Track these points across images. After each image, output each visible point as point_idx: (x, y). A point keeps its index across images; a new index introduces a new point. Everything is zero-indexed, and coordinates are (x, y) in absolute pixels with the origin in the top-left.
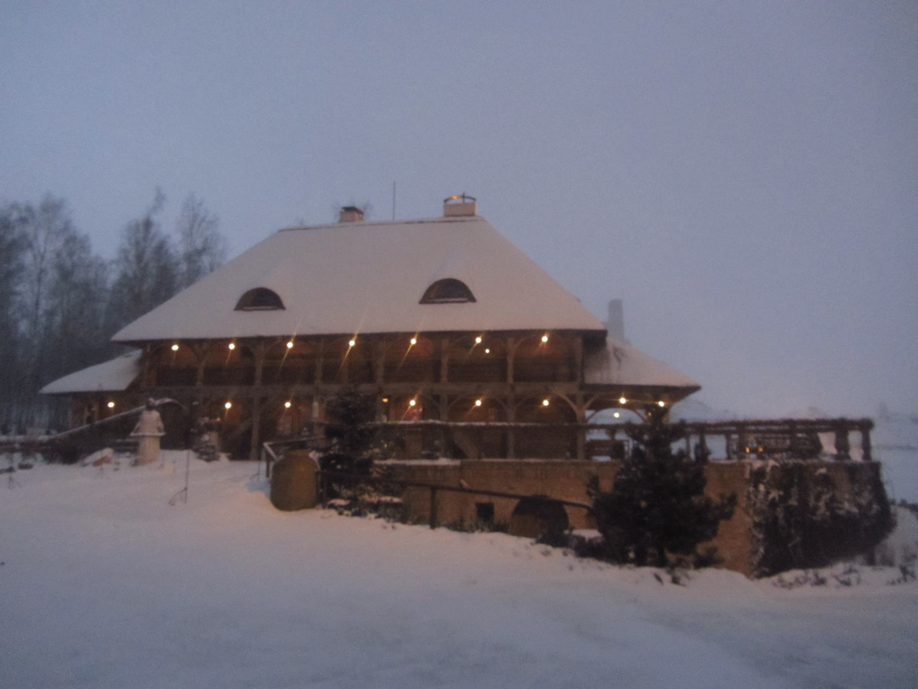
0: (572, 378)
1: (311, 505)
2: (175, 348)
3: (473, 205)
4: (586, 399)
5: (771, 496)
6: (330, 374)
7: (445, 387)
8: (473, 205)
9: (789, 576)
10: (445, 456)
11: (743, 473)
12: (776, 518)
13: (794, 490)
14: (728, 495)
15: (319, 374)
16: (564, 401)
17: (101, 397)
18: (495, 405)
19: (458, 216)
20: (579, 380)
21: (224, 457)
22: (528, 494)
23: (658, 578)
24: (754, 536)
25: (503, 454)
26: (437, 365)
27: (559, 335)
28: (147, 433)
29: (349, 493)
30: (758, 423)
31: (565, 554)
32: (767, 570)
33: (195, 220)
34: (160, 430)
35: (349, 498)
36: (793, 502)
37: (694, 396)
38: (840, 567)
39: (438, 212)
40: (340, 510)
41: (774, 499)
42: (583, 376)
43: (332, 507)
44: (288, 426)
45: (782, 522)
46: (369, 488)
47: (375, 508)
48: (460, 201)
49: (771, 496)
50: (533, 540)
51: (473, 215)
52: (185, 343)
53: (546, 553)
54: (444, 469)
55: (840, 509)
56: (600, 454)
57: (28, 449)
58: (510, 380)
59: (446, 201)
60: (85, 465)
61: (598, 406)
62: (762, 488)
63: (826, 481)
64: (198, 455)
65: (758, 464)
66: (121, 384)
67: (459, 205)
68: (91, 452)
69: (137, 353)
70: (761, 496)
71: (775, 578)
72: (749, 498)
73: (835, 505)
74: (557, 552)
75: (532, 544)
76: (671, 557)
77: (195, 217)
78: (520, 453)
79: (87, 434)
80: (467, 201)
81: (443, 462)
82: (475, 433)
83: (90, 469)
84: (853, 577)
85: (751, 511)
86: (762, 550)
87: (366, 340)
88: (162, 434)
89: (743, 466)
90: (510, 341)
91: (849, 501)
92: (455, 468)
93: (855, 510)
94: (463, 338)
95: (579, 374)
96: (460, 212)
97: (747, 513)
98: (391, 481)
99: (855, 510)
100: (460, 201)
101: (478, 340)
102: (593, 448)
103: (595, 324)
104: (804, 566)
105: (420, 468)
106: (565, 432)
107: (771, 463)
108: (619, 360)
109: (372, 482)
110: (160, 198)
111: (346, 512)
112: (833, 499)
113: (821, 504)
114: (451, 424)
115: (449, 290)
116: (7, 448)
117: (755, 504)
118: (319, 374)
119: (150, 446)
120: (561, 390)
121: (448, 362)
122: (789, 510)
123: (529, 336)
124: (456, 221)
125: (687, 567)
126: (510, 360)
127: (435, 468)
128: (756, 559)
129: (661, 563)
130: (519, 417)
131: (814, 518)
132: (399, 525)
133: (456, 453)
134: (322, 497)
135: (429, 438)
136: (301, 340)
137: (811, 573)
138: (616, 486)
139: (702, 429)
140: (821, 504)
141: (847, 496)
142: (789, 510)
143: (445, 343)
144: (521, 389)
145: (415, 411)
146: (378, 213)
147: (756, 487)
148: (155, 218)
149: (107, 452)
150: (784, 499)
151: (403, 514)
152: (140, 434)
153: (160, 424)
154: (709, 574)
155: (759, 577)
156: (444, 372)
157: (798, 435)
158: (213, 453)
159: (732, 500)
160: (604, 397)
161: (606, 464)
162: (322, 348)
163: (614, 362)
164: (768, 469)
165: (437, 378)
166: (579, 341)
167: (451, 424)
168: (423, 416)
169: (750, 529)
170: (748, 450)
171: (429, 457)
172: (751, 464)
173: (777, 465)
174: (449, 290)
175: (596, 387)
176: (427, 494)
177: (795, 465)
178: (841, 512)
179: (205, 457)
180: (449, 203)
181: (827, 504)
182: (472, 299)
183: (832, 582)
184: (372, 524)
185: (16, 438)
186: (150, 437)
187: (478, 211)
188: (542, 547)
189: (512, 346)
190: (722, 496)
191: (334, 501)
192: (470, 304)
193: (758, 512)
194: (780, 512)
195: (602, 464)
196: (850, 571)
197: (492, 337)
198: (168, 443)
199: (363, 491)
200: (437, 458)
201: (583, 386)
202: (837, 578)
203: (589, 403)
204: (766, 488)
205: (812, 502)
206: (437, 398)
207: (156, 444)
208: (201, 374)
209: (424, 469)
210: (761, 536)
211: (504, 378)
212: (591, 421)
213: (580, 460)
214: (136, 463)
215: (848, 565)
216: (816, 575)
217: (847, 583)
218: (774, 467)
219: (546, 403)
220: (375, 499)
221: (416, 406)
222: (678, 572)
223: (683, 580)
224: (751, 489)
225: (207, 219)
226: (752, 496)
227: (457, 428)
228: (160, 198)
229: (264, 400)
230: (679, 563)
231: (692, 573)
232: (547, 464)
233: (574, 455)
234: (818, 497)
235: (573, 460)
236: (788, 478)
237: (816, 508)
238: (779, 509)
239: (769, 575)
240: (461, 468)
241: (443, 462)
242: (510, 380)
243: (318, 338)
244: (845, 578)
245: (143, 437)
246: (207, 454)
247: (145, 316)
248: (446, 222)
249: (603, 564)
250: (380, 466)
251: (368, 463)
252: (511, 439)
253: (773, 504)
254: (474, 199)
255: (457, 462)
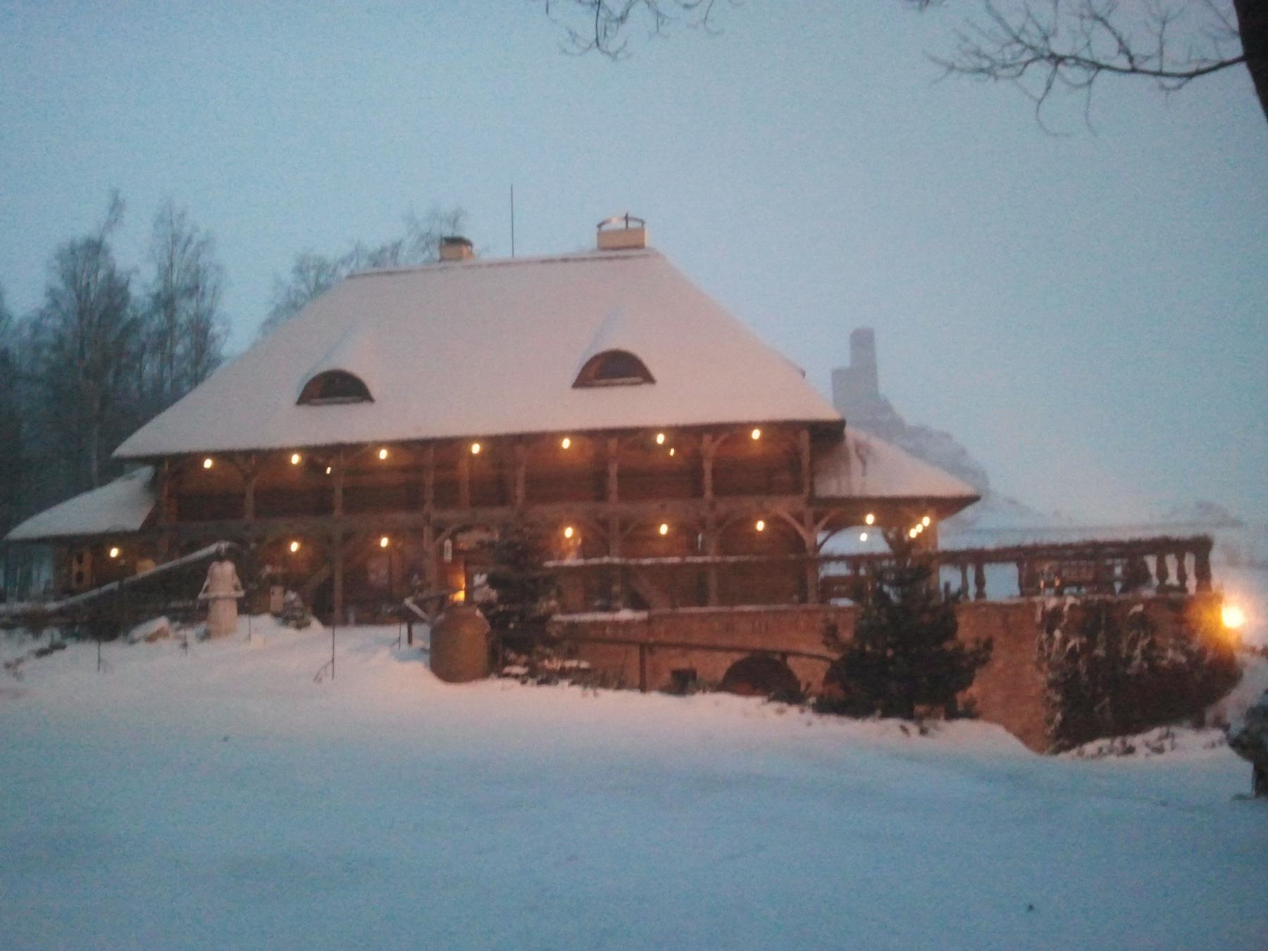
0: (796, 489)
1: (485, 675)
2: (208, 464)
3: (641, 231)
4: (816, 522)
5: (1070, 645)
6: (447, 494)
7: (614, 507)
8: (642, 230)
9: (1090, 748)
10: (626, 606)
11: (1033, 615)
12: (1076, 674)
13: (1101, 636)
14: (984, 638)
15: (429, 495)
16: (784, 521)
17: (99, 542)
18: (685, 531)
19: (618, 248)
20: (807, 490)
21: (316, 624)
22: (758, 646)
23: (904, 729)
24: (1048, 698)
25: (703, 603)
26: (599, 477)
27: (777, 429)
28: (221, 594)
29: (524, 658)
30: (1054, 547)
31: (802, 711)
32: (1067, 743)
33: (176, 241)
34: (236, 589)
35: (525, 665)
36: (1100, 652)
37: (968, 512)
38: (1154, 734)
39: (589, 240)
40: (523, 680)
41: (1074, 648)
42: (812, 484)
43: (507, 675)
44: (383, 572)
45: (1085, 679)
46: (548, 651)
47: (563, 674)
48: (622, 225)
49: (1070, 645)
50: (765, 699)
51: (640, 246)
52: (222, 456)
53: (781, 712)
54: (628, 624)
55: (1163, 659)
56: (840, 595)
57: (34, 623)
58: (708, 494)
59: (600, 226)
60: (133, 642)
61: (835, 527)
62: (1057, 634)
63: (1142, 621)
64: (281, 620)
65: (1052, 603)
66: (133, 521)
67: (619, 232)
68: (137, 622)
69: (146, 472)
70: (1056, 645)
71: (1074, 752)
72: (1041, 648)
73: (1155, 653)
74: (793, 711)
75: (763, 703)
76: (920, 709)
77: (175, 239)
78: (727, 598)
79: (106, 600)
80: (632, 225)
81: (625, 615)
82: (657, 573)
83: (142, 646)
84: (1167, 743)
85: (1045, 667)
86: (1059, 716)
87: (495, 443)
88: (241, 594)
89: (1033, 606)
90: (707, 438)
91: (1175, 648)
92: (643, 622)
93: (1183, 659)
94: (636, 437)
95: (807, 480)
96: (623, 243)
97: (1040, 669)
98: (575, 640)
99: (1183, 659)
100: (622, 225)
101: (660, 439)
102: (829, 588)
103: (826, 411)
104: (1112, 733)
105: (594, 624)
106: (792, 565)
107: (1070, 600)
108: (864, 462)
109: (551, 642)
110: (117, 206)
111: (530, 681)
112: (1152, 645)
113: (1137, 652)
114: (632, 562)
115: (615, 368)
116: (10, 624)
117: (1049, 655)
118: (429, 495)
119: (226, 612)
120: (783, 507)
121: (618, 470)
122: (1094, 664)
123: (733, 432)
124: (617, 257)
125: (937, 717)
126: (708, 466)
127: (616, 625)
128: (1050, 730)
129: (908, 715)
130: (724, 549)
131: (1129, 672)
132: (601, 691)
133: (637, 603)
134: (495, 666)
135: (599, 586)
136: (398, 446)
137: (1117, 742)
138: (856, 634)
139: (978, 558)
140: (1137, 652)
141: (1171, 641)
142: (1094, 664)
143: (613, 444)
144: (722, 507)
145: (571, 543)
146: (489, 243)
147: (1050, 632)
148: (108, 239)
149: (162, 622)
150: (1087, 648)
151: (597, 678)
152: (213, 595)
153: (236, 580)
154: (962, 725)
155: (1057, 751)
156: (613, 485)
157: (1088, 558)
158: (303, 617)
159: (988, 645)
160: (844, 513)
161: (849, 609)
162: (431, 459)
163: (855, 463)
164: (1066, 609)
165: (601, 496)
166: (805, 436)
167: (632, 562)
168: (584, 551)
169: (1044, 691)
170: (1042, 584)
171: (606, 609)
172: (1043, 604)
173: (1078, 602)
174: (615, 368)
175: (832, 502)
176: (635, 652)
177: (1100, 601)
178: (1164, 663)
179: (293, 622)
180: (605, 228)
181: (1143, 652)
182: (648, 378)
183: (1142, 751)
184: (565, 695)
185: (18, 607)
186: (225, 598)
187: (649, 241)
188: (776, 705)
189: (709, 446)
190: (977, 641)
191: (507, 670)
192: (646, 388)
193: (1052, 667)
194: (1082, 665)
195: (840, 610)
196: (1167, 736)
197: (680, 434)
198: (247, 607)
199: (544, 656)
200: (617, 610)
201: (812, 500)
202: (1147, 745)
203: (823, 523)
204: (1063, 632)
205: (1124, 651)
206: (604, 524)
207: (232, 608)
208: (250, 503)
209: (603, 625)
210: (1058, 698)
211: (698, 493)
212: (825, 550)
213: (812, 605)
214: (207, 636)
215: (1164, 730)
216: (1124, 743)
217: (1160, 750)
218: (1072, 607)
219: (760, 526)
220: (556, 664)
221: (574, 537)
222: (926, 723)
223: (932, 730)
224: (1044, 636)
225: (195, 240)
226: (1046, 647)
227: (641, 567)
228: (117, 206)
229: (347, 536)
230: (928, 715)
231: (942, 723)
232: (767, 612)
233: (804, 600)
234: (1133, 644)
235: (803, 606)
236: (1095, 620)
237: (1130, 658)
238: (1080, 662)
239: (1067, 748)
240: (649, 622)
241: (625, 615)
242: (708, 494)
243: (425, 443)
244: (1157, 745)
245: (216, 599)
246: (294, 618)
247: (163, 415)
248: (600, 258)
249: (845, 720)
250: (560, 623)
251: (544, 619)
252: (713, 582)
253: (1073, 655)
254: (643, 222)
255: (642, 615)
